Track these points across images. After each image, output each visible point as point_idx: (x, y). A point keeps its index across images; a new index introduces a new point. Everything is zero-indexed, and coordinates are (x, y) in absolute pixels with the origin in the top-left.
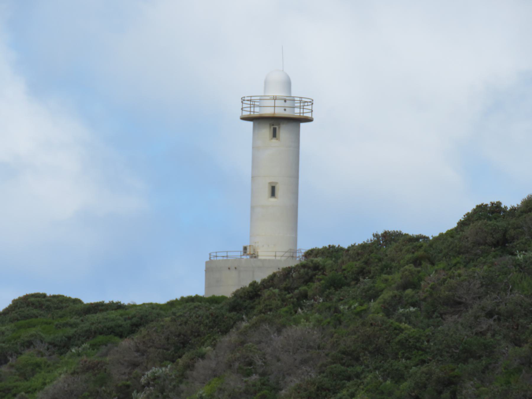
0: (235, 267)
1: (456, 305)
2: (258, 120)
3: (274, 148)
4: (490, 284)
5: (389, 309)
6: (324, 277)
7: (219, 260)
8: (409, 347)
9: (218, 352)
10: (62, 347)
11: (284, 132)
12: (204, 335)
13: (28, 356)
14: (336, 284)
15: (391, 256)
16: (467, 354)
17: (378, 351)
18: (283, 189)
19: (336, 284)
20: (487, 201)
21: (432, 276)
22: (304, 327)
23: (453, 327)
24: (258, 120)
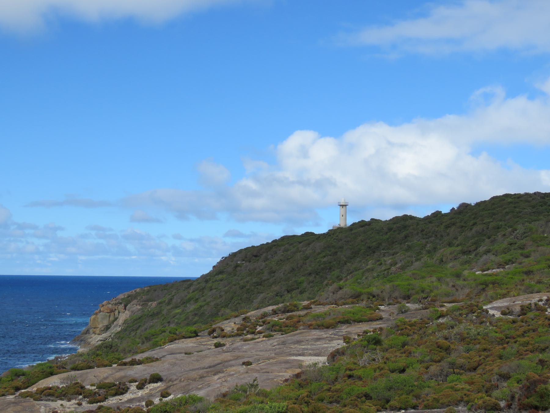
2: (340, 205)
24: (340, 205)
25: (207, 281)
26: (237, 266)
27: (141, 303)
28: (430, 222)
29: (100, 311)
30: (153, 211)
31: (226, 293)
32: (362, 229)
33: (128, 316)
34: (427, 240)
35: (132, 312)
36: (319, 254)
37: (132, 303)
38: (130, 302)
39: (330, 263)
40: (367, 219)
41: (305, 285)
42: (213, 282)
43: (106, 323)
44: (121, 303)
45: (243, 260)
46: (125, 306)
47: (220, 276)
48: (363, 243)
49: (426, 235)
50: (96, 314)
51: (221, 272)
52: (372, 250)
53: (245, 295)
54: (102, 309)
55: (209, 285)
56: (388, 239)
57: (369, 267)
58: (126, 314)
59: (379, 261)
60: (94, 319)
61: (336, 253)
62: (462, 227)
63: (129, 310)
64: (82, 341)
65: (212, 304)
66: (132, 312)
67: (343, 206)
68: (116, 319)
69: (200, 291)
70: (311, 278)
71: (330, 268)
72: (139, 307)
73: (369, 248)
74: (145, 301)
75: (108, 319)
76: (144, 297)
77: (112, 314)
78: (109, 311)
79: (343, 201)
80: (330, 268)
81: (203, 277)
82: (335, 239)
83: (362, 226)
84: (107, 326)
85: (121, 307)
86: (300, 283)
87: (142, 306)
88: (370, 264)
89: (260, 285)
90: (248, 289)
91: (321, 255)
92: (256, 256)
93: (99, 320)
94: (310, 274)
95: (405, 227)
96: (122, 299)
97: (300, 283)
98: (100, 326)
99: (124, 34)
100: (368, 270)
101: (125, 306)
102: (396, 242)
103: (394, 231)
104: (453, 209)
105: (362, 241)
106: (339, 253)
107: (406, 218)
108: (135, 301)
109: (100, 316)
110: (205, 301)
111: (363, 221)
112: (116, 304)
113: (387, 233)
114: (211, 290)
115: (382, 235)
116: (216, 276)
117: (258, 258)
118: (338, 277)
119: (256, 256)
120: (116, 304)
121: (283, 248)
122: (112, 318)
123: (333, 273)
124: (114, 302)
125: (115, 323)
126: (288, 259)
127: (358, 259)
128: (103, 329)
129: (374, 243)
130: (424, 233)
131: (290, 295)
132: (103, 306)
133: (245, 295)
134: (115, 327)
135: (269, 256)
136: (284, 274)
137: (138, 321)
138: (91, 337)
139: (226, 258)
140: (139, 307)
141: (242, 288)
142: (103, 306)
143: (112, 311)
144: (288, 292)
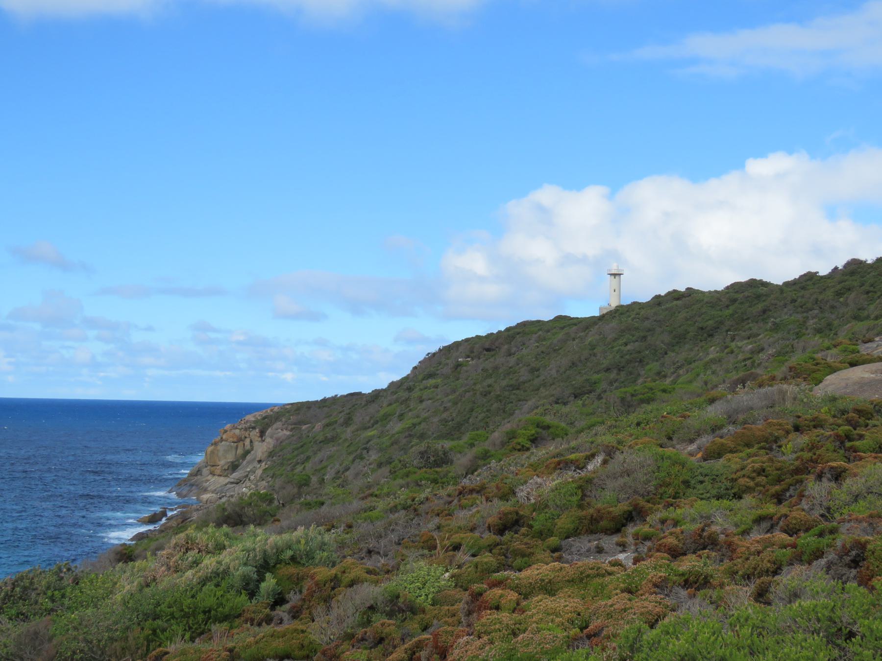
0: (606, 308)
1: (647, 319)
2: (611, 274)
3: (615, 281)
4: (655, 314)
5: (633, 320)
6: (620, 312)
7: (159, 497)
8: (637, 329)
9: (594, 330)
10: (562, 328)
11: (617, 277)
12: (705, 401)
13: (554, 330)
14: (622, 314)
15: (636, 306)
16: (649, 330)
17: (630, 330)
18: (617, 290)
19: (622, 314)
20: (671, 290)
21: (643, 312)
22: (614, 324)
23: (647, 324)
24: (611, 274)
25: (410, 389)
26: (458, 366)
27: (290, 427)
28: (803, 288)
29: (222, 440)
30: (277, 293)
31: (456, 403)
32: (679, 302)
33: (271, 446)
34: (805, 315)
35: (277, 439)
36: (615, 340)
37: (275, 426)
38: (268, 426)
39: (639, 352)
40: (682, 289)
41: (603, 385)
42: (421, 390)
43: (230, 458)
44: (254, 428)
45: (468, 357)
46: (262, 434)
47: (432, 382)
48: (689, 322)
49: (801, 307)
50: (216, 444)
51: (431, 376)
52: (708, 333)
53: (495, 405)
54: (224, 437)
55: (416, 394)
56: (732, 315)
57: (711, 356)
58: (268, 443)
59: (727, 347)
60: (212, 452)
61: (644, 338)
62: (868, 293)
63: (271, 437)
64: (192, 485)
65: (436, 420)
66: (277, 439)
67: (615, 275)
68: (247, 453)
69: (401, 404)
70: (613, 375)
71: (641, 361)
72: (288, 433)
73: (702, 329)
74: (295, 424)
75: (234, 452)
76: (293, 419)
77: (241, 444)
78: (235, 440)
79: (615, 268)
80: (641, 361)
81: (395, 387)
82: (635, 318)
83: (678, 299)
84: (232, 462)
85: (255, 433)
86: (595, 383)
87: (291, 430)
88: (713, 352)
89: (518, 389)
90: (499, 396)
91: (621, 342)
92: (488, 350)
93: (220, 454)
94: (608, 370)
95: (758, 297)
96: (256, 422)
97: (595, 383)
98: (222, 462)
99: (110, 34)
100: (713, 361)
101: (262, 434)
102: (748, 319)
103: (742, 303)
104: (836, 268)
105: (687, 319)
106: (649, 338)
107: (753, 284)
108: (278, 424)
109: (222, 447)
110: (418, 417)
111: (675, 291)
112: (246, 429)
113: (727, 306)
114: (421, 401)
115: (721, 310)
116: (424, 382)
117: (492, 353)
118: (659, 373)
119: (488, 350)
120: (246, 429)
121: (535, 336)
122: (240, 451)
123: (648, 367)
124: (244, 426)
125: (248, 457)
126: (555, 350)
127: (687, 346)
128: (226, 467)
129: (710, 322)
130: (797, 304)
131: (580, 402)
132: (226, 431)
133: (495, 405)
134: (249, 463)
135: (514, 349)
136: (558, 371)
137: (300, 450)
138: (208, 481)
139: (434, 354)
140: (288, 433)
141: (485, 395)
142: (226, 431)
143: (240, 440)
144: (575, 397)
